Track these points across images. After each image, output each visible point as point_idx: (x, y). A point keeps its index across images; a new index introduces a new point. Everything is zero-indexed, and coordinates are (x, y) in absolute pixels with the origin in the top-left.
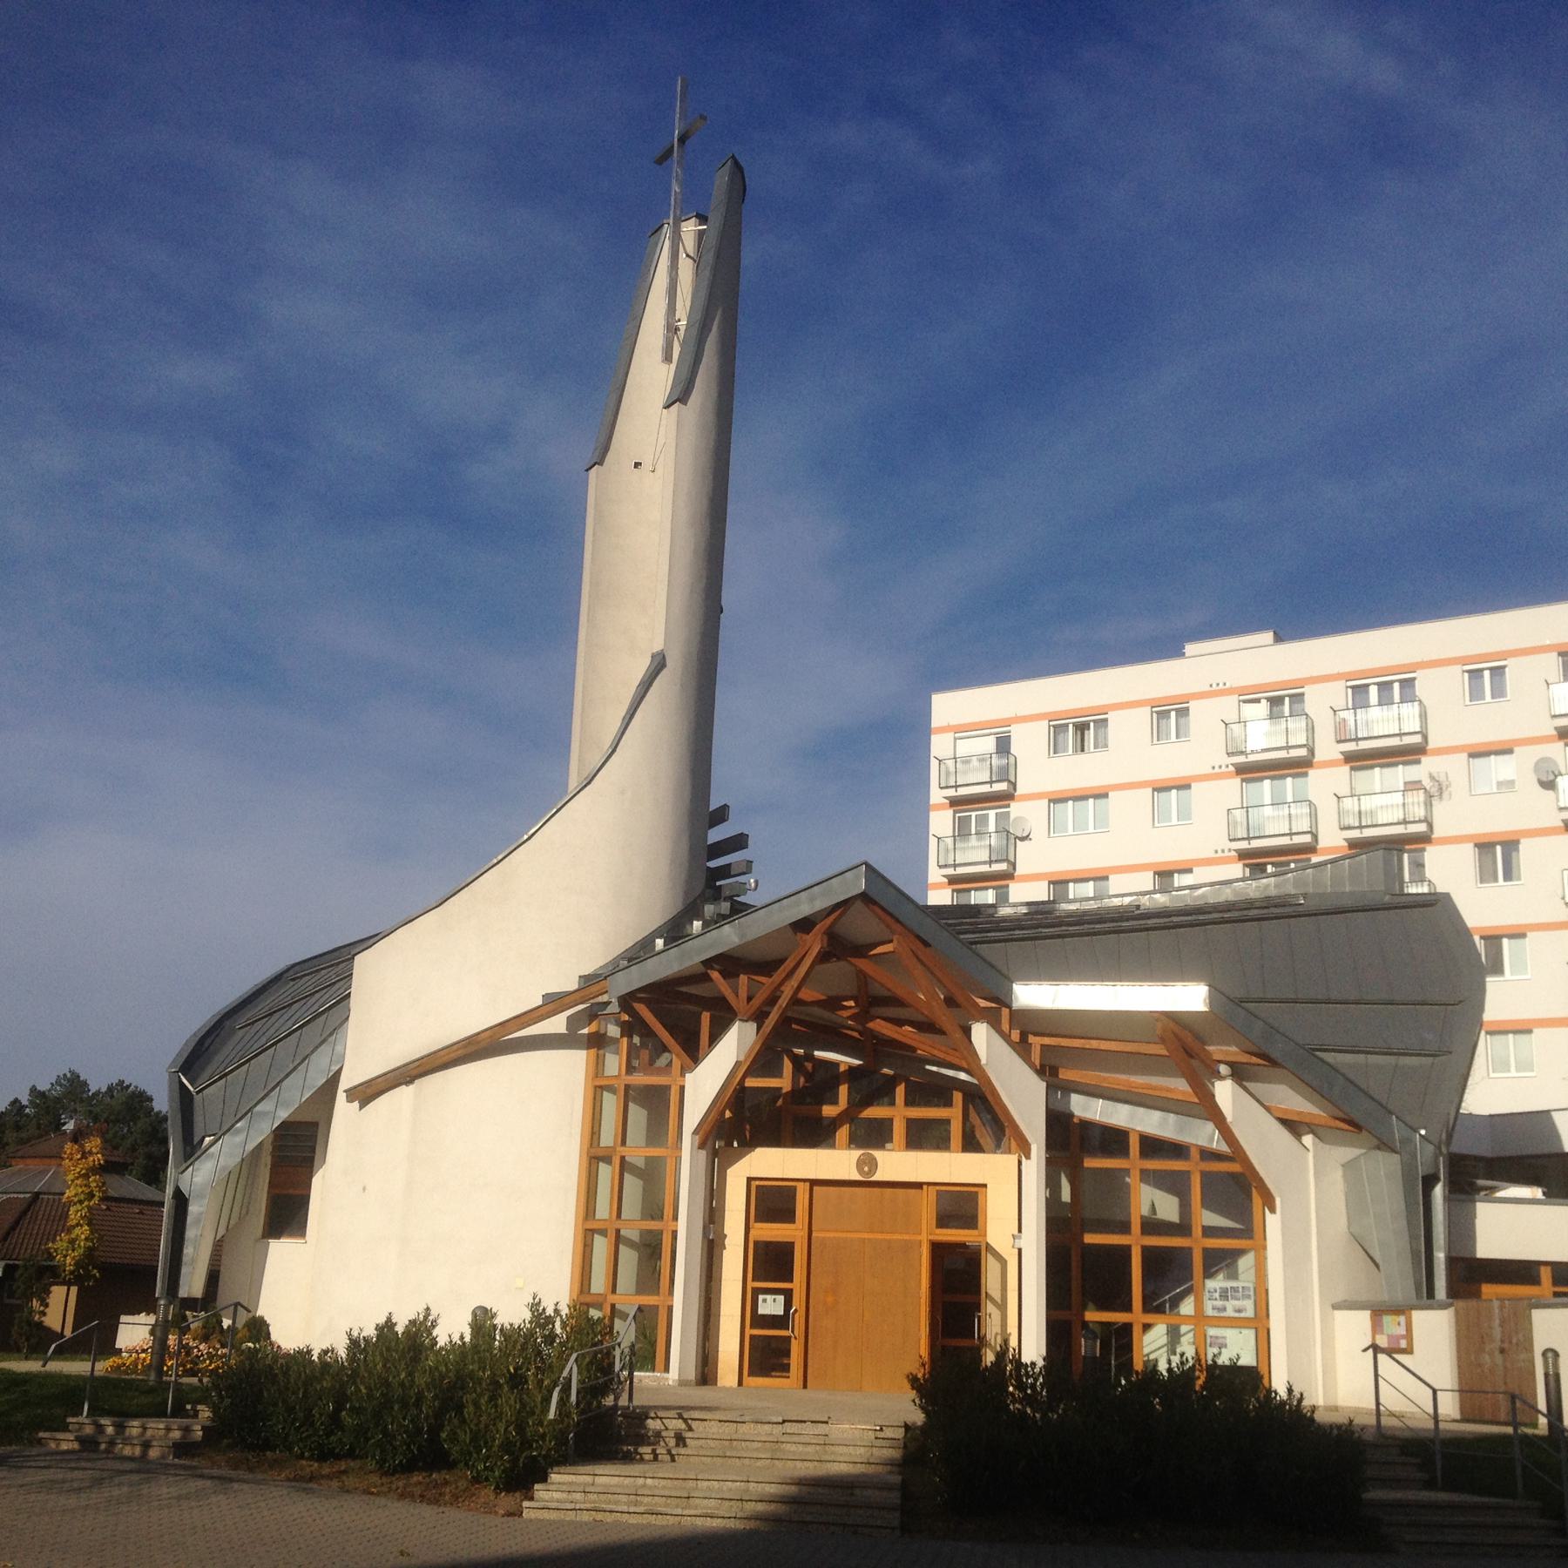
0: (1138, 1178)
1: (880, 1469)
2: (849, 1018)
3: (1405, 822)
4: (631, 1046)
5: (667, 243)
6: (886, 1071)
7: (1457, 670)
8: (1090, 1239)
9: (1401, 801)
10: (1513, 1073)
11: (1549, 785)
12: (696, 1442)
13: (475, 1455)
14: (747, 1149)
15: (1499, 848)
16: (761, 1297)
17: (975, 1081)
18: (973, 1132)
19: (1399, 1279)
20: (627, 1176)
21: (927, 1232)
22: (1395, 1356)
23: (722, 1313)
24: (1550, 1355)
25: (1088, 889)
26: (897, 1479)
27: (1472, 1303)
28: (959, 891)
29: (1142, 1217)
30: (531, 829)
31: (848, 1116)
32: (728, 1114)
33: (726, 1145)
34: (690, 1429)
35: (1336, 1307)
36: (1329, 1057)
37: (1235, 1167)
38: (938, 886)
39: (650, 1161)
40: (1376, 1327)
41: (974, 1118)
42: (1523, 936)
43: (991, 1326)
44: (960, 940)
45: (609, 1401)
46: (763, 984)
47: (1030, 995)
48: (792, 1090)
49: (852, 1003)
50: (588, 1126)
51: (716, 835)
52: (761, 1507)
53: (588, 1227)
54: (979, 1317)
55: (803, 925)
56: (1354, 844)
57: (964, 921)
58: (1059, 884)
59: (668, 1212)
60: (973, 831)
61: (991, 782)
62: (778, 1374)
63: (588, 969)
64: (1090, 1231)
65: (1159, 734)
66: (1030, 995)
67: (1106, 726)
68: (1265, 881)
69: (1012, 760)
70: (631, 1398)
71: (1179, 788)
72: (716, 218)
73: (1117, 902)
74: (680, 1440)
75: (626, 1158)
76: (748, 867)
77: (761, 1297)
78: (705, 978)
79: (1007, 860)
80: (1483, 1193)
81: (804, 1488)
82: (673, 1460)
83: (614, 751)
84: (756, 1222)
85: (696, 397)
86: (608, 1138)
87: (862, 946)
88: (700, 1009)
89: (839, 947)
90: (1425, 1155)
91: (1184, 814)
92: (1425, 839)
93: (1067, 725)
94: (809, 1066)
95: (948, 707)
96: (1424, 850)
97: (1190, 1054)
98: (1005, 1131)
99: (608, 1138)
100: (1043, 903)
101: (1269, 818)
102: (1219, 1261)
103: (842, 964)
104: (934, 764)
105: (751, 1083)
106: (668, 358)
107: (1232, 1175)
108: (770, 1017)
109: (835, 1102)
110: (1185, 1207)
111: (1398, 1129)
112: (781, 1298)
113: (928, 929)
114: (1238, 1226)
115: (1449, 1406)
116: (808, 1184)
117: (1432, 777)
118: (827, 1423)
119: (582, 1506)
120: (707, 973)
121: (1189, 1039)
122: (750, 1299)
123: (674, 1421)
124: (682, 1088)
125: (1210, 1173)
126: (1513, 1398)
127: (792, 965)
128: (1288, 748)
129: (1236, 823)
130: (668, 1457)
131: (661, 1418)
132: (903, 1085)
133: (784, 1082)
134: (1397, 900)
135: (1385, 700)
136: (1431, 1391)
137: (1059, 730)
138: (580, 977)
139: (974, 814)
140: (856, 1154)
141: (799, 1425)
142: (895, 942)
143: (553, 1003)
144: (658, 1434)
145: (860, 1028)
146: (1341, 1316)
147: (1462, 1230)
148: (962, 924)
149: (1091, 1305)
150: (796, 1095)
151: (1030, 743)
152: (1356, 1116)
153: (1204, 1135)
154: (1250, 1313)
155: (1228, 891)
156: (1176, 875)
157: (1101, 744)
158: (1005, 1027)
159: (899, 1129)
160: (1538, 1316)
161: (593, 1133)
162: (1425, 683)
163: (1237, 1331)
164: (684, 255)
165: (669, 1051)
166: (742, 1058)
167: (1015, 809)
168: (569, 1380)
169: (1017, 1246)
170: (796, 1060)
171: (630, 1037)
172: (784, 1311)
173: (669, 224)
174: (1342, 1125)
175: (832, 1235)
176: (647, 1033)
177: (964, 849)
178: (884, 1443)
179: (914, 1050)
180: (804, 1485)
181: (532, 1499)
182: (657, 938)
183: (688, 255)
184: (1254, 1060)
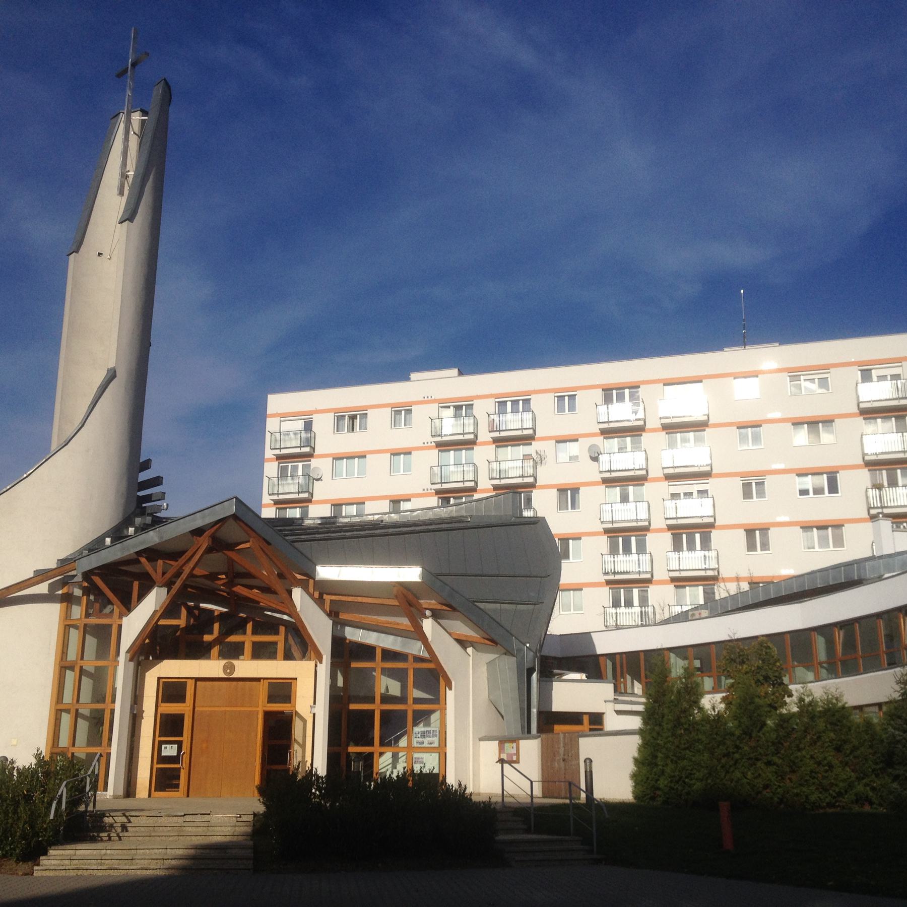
0: (380, 672)
1: (240, 838)
2: (223, 585)
3: (523, 476)
4: (88, 601)
5: (122, 126)
6: (242, 615)
7: (552, 395)
8: (353, 707)
9: (521, 465)
10: (572, 612)
11: (595, 459)
12: (134, 829)
13: (4, 842)
14: (159, 661)
15: (569, 492)
16: (163, 746)
17: (293, 621)
18: (290, 648)
19: (514, 724)
20: (83, 678)
21: (262, 705)
22: (513, 764)
23: (140, 756)
24: (588, 761)
25: (353, 510)
26: (251, 843)
27: (550, 735)
28: (279, 509)
29: (381, 694)
30: (28, 471)
31: (218, 641)
32: (147, 641)
33: (145, 659)
34: (130, 822)
35: (481, 739)
36: (482, 605)
37: (431, 666)
38: (268, 506)
39: (97, 668)
40: (501, 749)
41: (291, 641)
42: (580, 539)
43: (296, 756)
44: (287, 540)
45: (82, 808)
46: (172, 566)
47: (326, 572)
48: (186, 626)
49: (224, 576)
50: (61, 648)
51: (143, 476)
52: (174, 862)
53: (59, 708)
54: (290, 753)
55: (198, 532)
56: (496, 488)
57: (286, 528)
58: (337, 506)
59: (108, 698)
60: (289, 475)
61: (300, 447)
62: (170, 790)
63: (63, 556)
64: (353, 703)
65: (395, 423)
66: (326, 572)
67: (366, 417)
68: (450, 508)
69: (313, 435)
70: (94, 806)
71: (405, 454)
72: (154, 112)
73: (370, 518)
74: (124, 828)
75: (84, 667)
76: (162, 496)
77: (163, 746)
78: (139, 562)
79: (308, 492)
80: (556, 677)
81: (198, 851)
82: (120, 840)
83: (83, 426)
84: (162, 702)
85: (139, 218)
86: (72, 655)
87: (231, 544)
88: (132, 579)
89: (219, 545)
90: (529, 658)
91: (407, 468)
92: (532, 486)
93: (344, 416)
94: (196, 612)
95: (277, 402)
96: (532, 492)
97: (410, 605)
98: (308, 648)
99: (72, 655)
100: (329, 518)
101: (452, 472)
102: (422, 717)
103: (220, 554)
104: (268, 435)
105: (163, 622)
106: (121, 193)
107: (430, 670)
108: (176, 584)
109: (211, 633)
110: (404, 688)
111: (515, 644)
112: (175, 746)
113: (269, 534)
114: (432, 697)
115: (538, 791)
116: (194, 680)
117: (537, 453)
118: (209, 814)
119: (70, 867)
120: (138, 559)
121: (411, 597)
122: (157, 747)
123: (120, 818)
124: (120, 626)
125: (419, 669)
126: (570, 784)
127: (190, 555)
128: (463, 434)
129: (435, 474)
130: (117, 838)
131: (112, 817)
132: (251, 623)
133: (181, 622)
134: (518, 520)
135: (515, 410)
136: (530, 782)
137: (340, 418)
138: (58, 560)
139: (290, 465)
140: (223, 662)
141: (194, 816)
142: (251, 542)
143: (41, 576)
144: (111, 826)
145: (228, 590)
146: (483, 744)
147: (546, 696)
148: (285, 530)
149: (351, 743)
150: (188, 629)
151: (323, 425)
152: (496, 638)
153: (416, 648)
154: (436, 744)
155: (431, 513)
156: (402, 502)
157: (363, 427)
158: (311, 590)
159: (248, 648)
160: (583, 741)
161: (63, 653)
162: (536, 402)
163: (429, 754)
164: (132, 133)
165: (113, 604)
166: (158, 609)
167: (314, 462)
168: (61, 796)
169: (313, 712)
170: (190, 610)
171: (88, 596)
172: (177, 753)
173: (124, 113)
174: (487, 642)
175: (207, 709)
176: (99, 593)
177: (284, 485)
178: (241, 824)
179: (258, 602)
180: (199, 849)
181: (38, 865)
182: (107, 537)
183: (134, 133)
184: (444, 608)
